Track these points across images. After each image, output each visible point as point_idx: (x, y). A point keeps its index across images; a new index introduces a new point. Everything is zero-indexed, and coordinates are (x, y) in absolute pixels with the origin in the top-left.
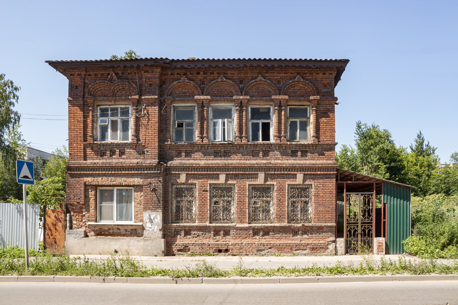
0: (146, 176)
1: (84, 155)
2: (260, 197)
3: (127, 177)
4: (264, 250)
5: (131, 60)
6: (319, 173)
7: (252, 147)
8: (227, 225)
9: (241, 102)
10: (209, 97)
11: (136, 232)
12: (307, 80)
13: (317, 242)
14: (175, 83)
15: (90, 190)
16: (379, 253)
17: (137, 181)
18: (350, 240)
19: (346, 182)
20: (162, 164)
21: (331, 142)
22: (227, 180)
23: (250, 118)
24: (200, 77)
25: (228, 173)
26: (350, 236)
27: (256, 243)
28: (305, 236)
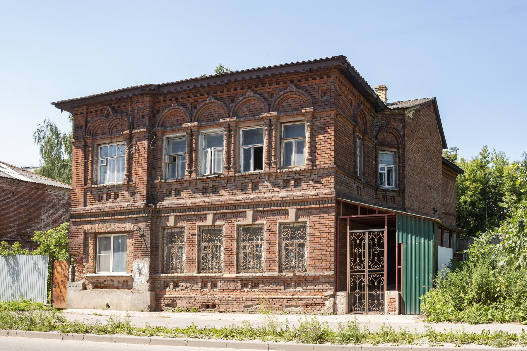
0: (136, 221)
1: (84, 201)
2: (249, 240)
3: (119, 223)
4: (252, 306)
5: (222, 75)
6: (314, 206)
7: (241, 179)
8: (213, 275)
9: (229, 125)
10: (196, 124)
11: (126, 284)
12: (301, 88)
13: (312, 297)
14: (166, 111)
15: (90, 239)
16: (391, 312)
17: (128, 226)
18: (372, 295)
19: (350, 217)
20: (150, 206)
21: (329, 165)
22: (214, 221)
23: (241, 143)
24: (191, 100)
25: (215, 212)
26: (355, 289)
27: (244, 297)
28: (299, 289)
